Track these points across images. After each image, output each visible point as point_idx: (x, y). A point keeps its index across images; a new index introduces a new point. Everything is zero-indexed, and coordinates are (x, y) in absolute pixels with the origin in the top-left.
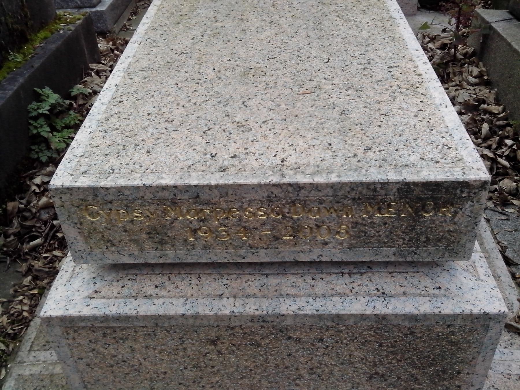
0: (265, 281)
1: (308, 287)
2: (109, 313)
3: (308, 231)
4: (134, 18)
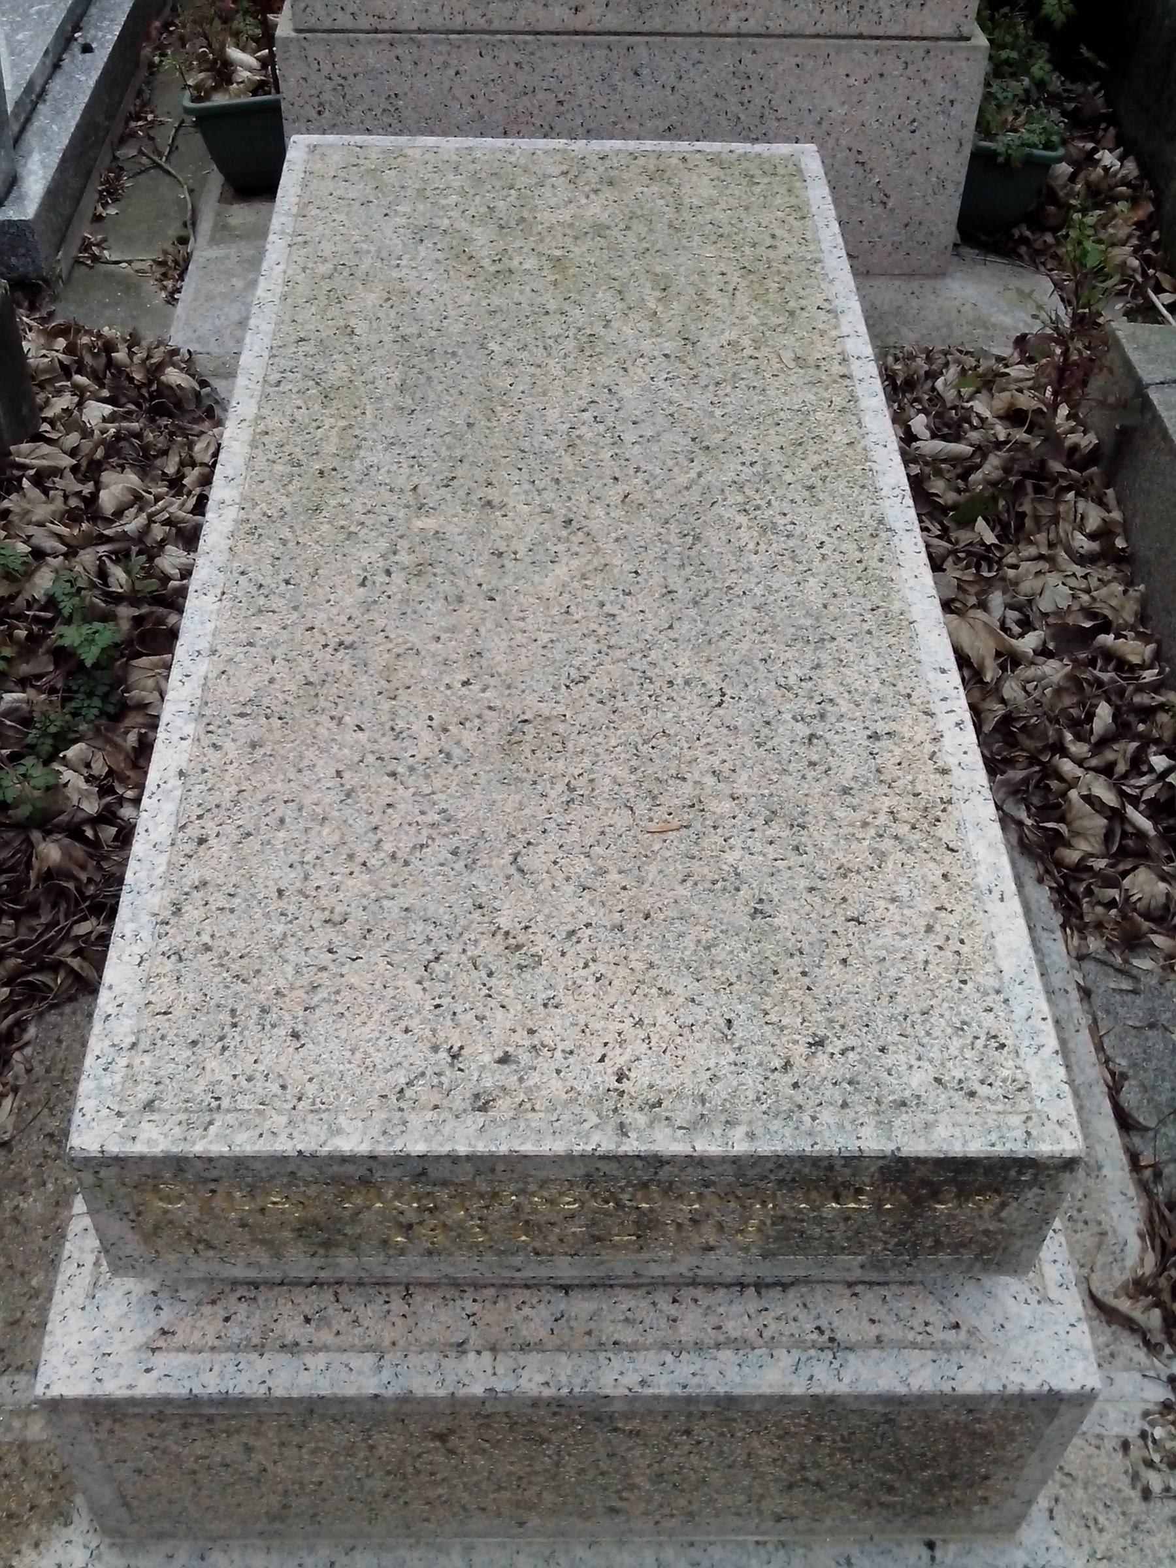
0: (562, 1307)
1: (663, 1323)
3: (671, 1229)
4: (112, 211)
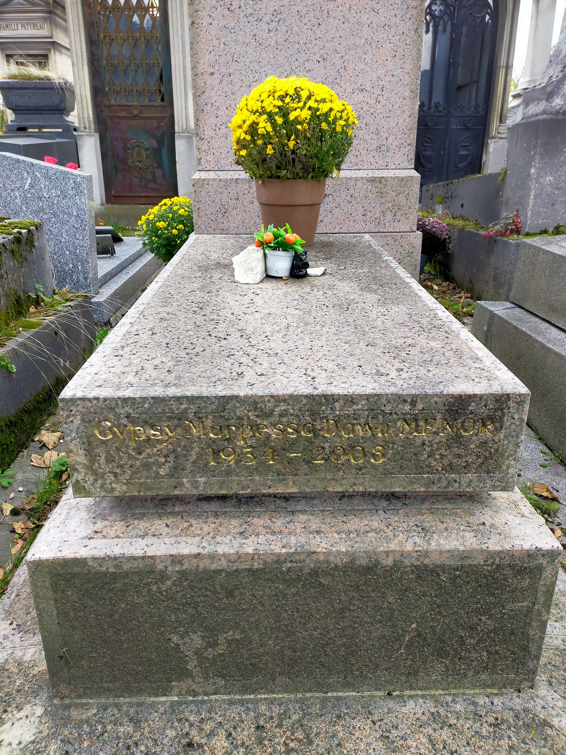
2: (111, 553)
